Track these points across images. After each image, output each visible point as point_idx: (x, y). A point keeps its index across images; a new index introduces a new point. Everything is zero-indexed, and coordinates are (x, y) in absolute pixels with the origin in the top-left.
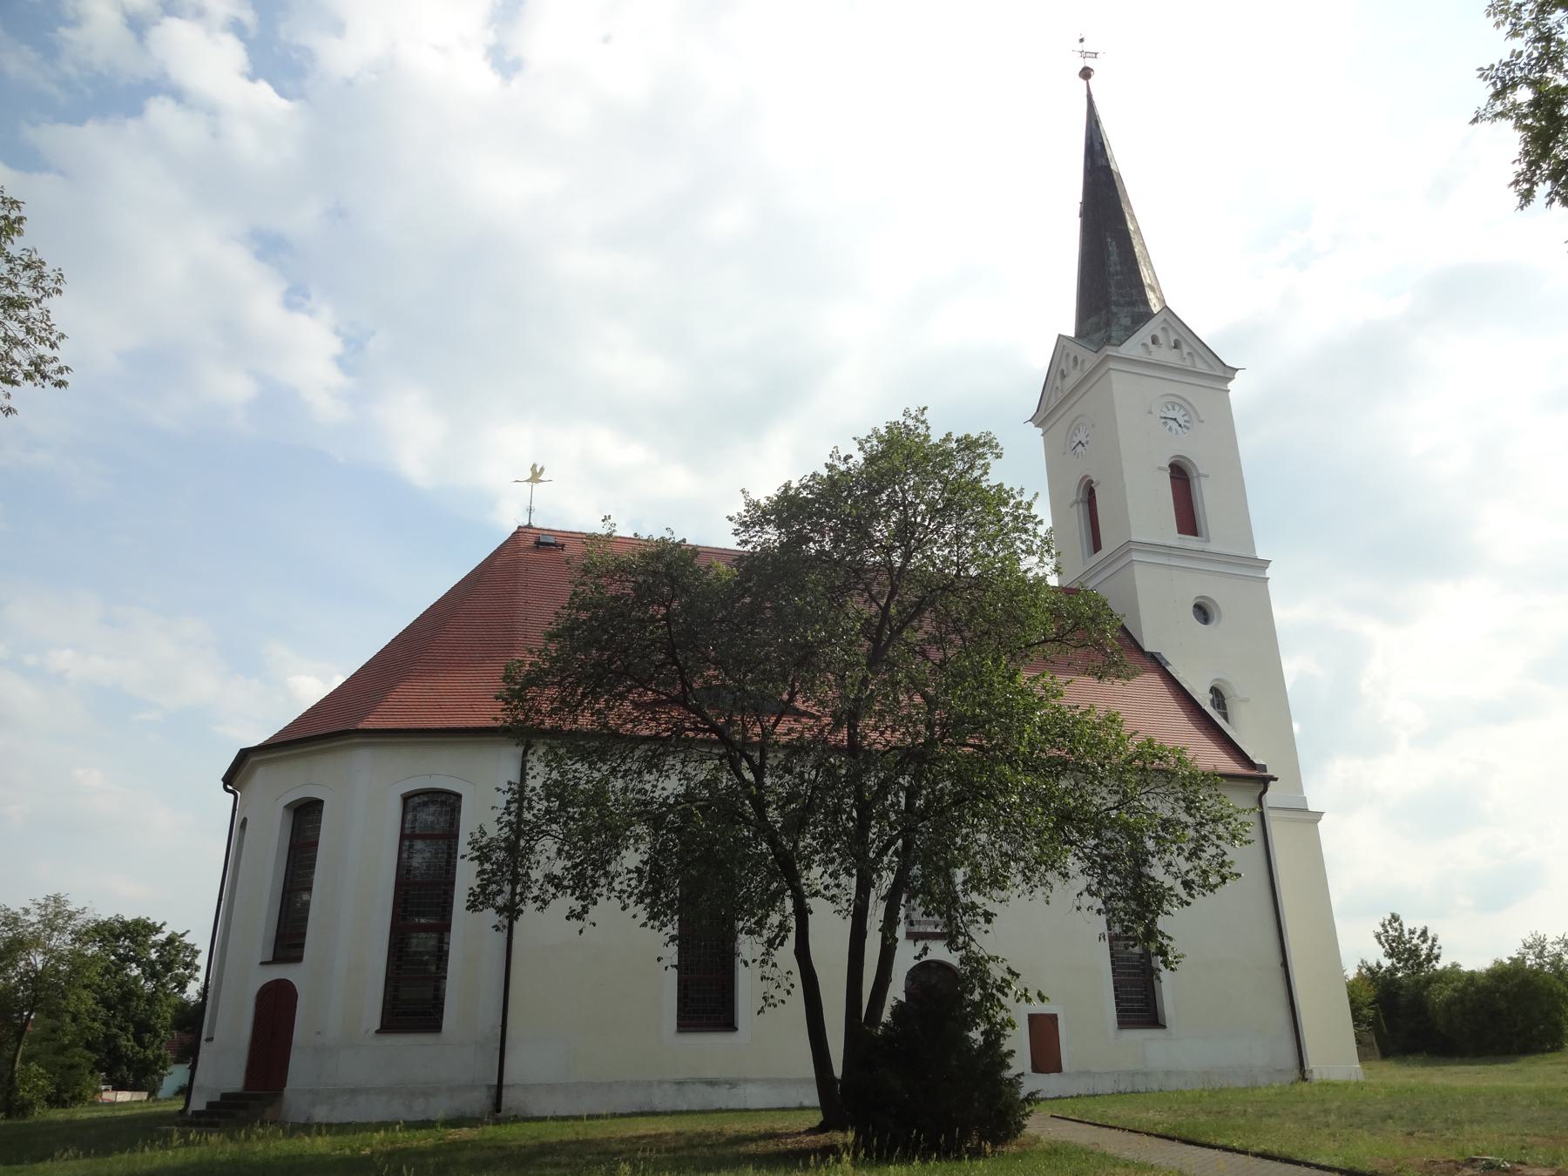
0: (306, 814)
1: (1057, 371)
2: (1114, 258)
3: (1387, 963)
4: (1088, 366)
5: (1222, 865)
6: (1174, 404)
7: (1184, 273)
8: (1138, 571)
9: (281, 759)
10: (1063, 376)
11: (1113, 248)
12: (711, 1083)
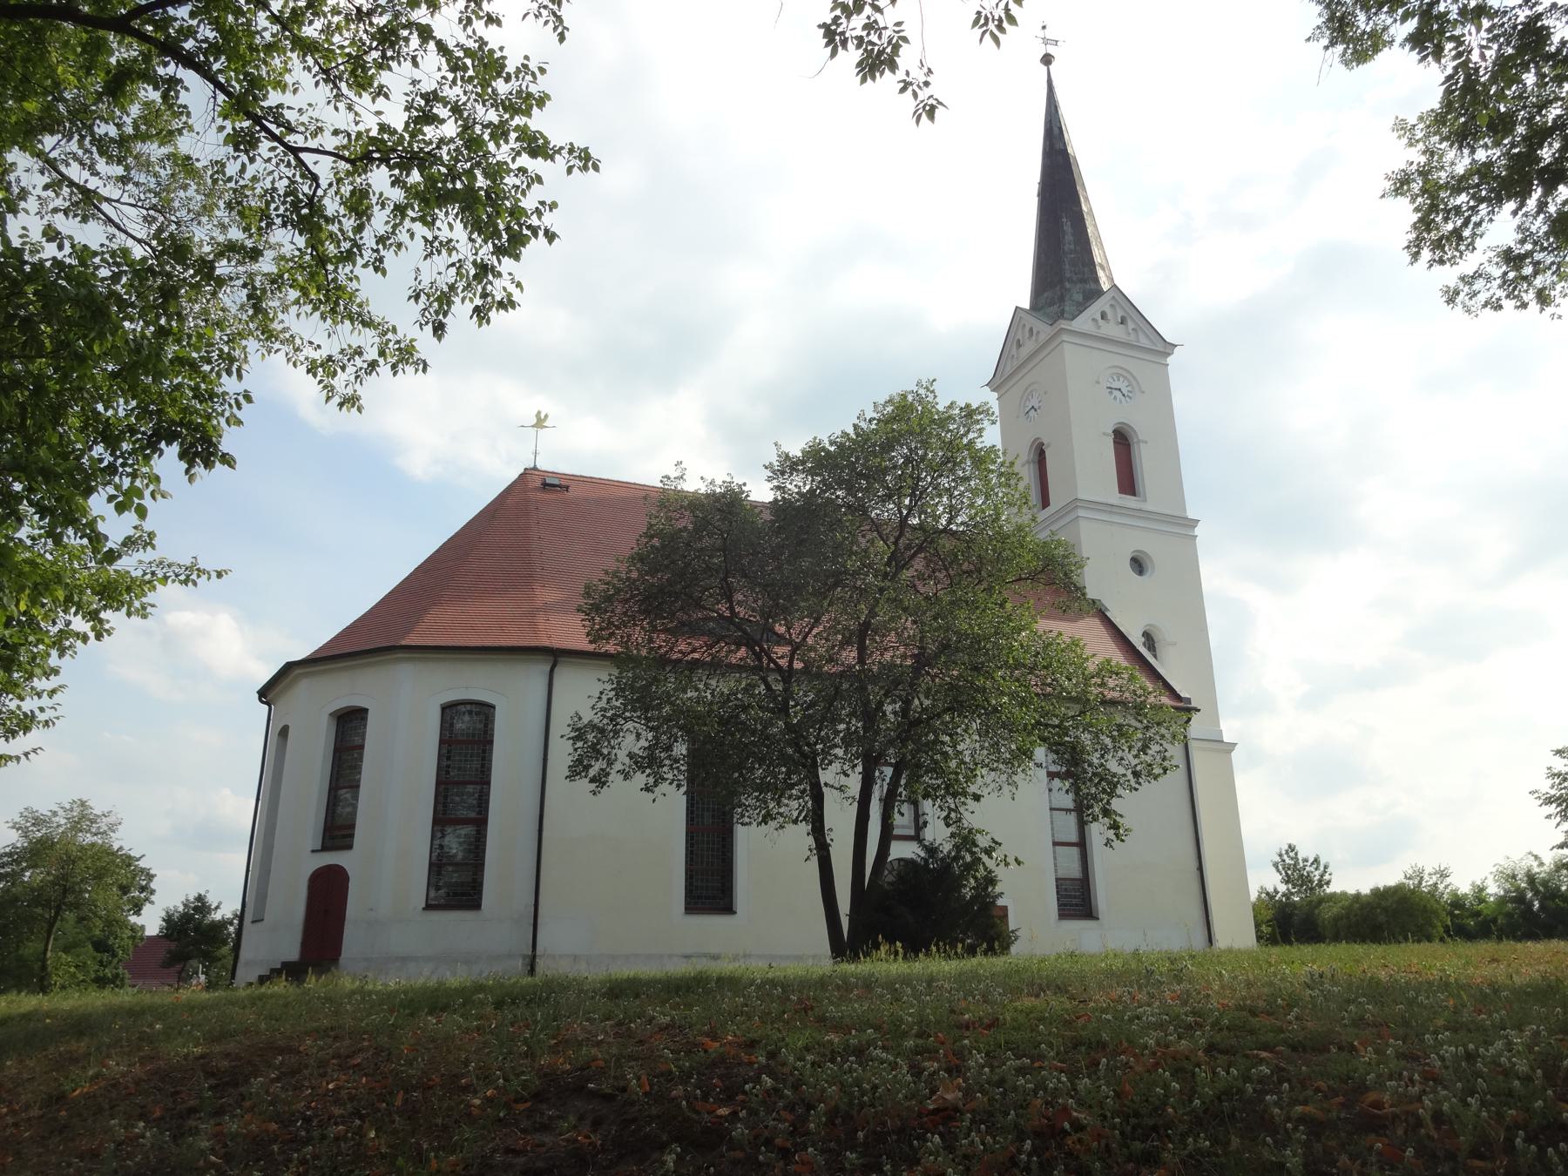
0: (350, 722)
1: (1012, 340)
2: (1069, 238)
3: (1282, 888)
4: (1043, 337)
5: (1164, 759)
6: (1119, 375)
7: (1124, 251)
8: (1083, 524)
9: (324, 672)
10: (1019, 345)
11: (1068, 228)
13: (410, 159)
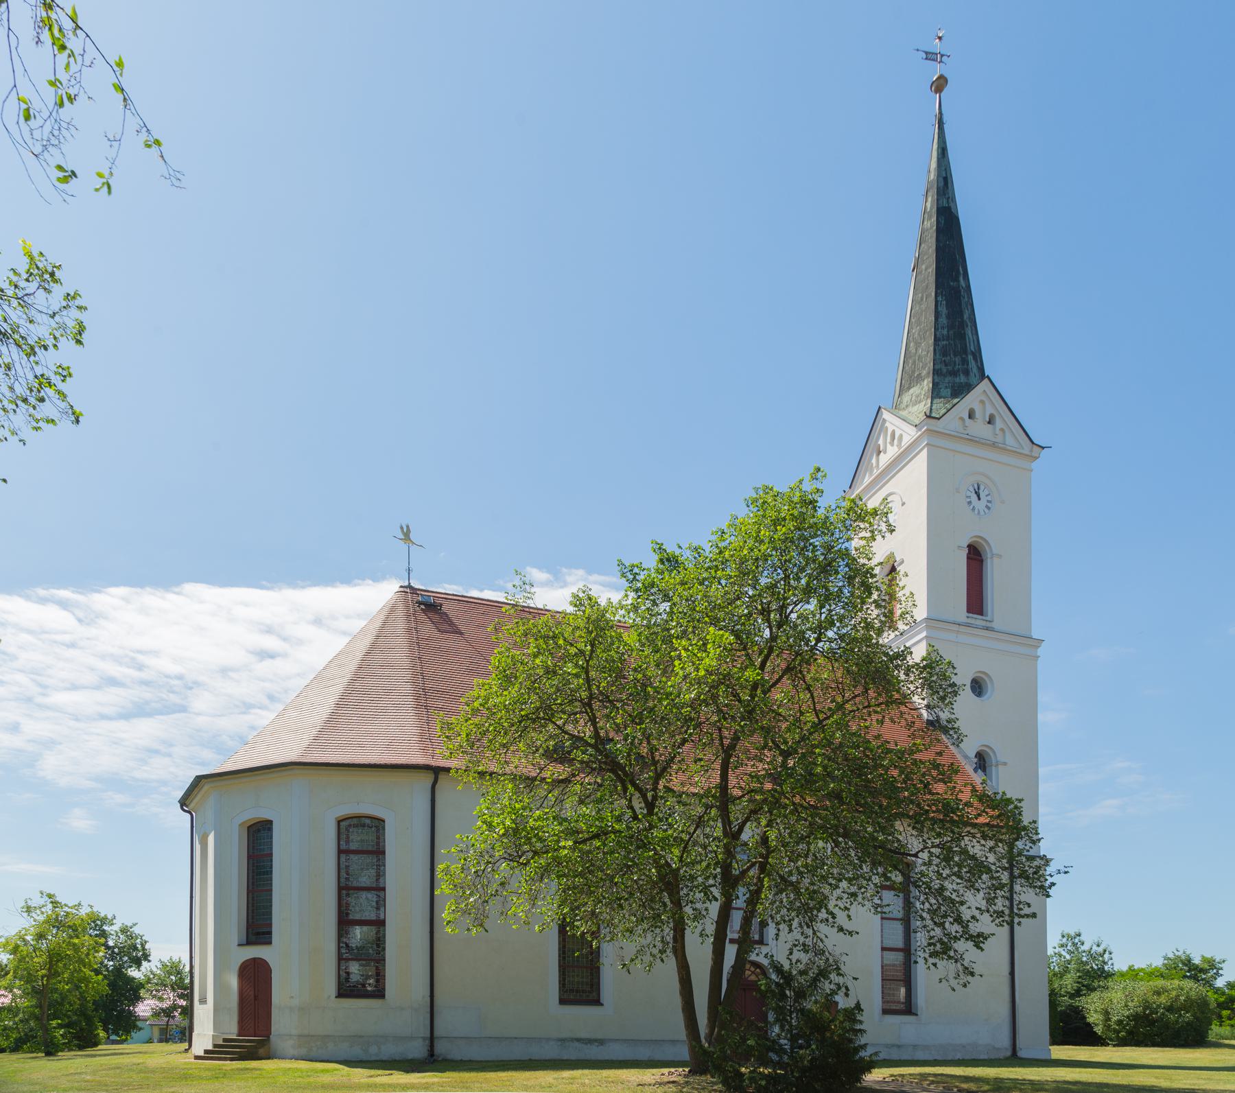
4: (907, 440)
12: (589, 1041)
13: (574, 888)
